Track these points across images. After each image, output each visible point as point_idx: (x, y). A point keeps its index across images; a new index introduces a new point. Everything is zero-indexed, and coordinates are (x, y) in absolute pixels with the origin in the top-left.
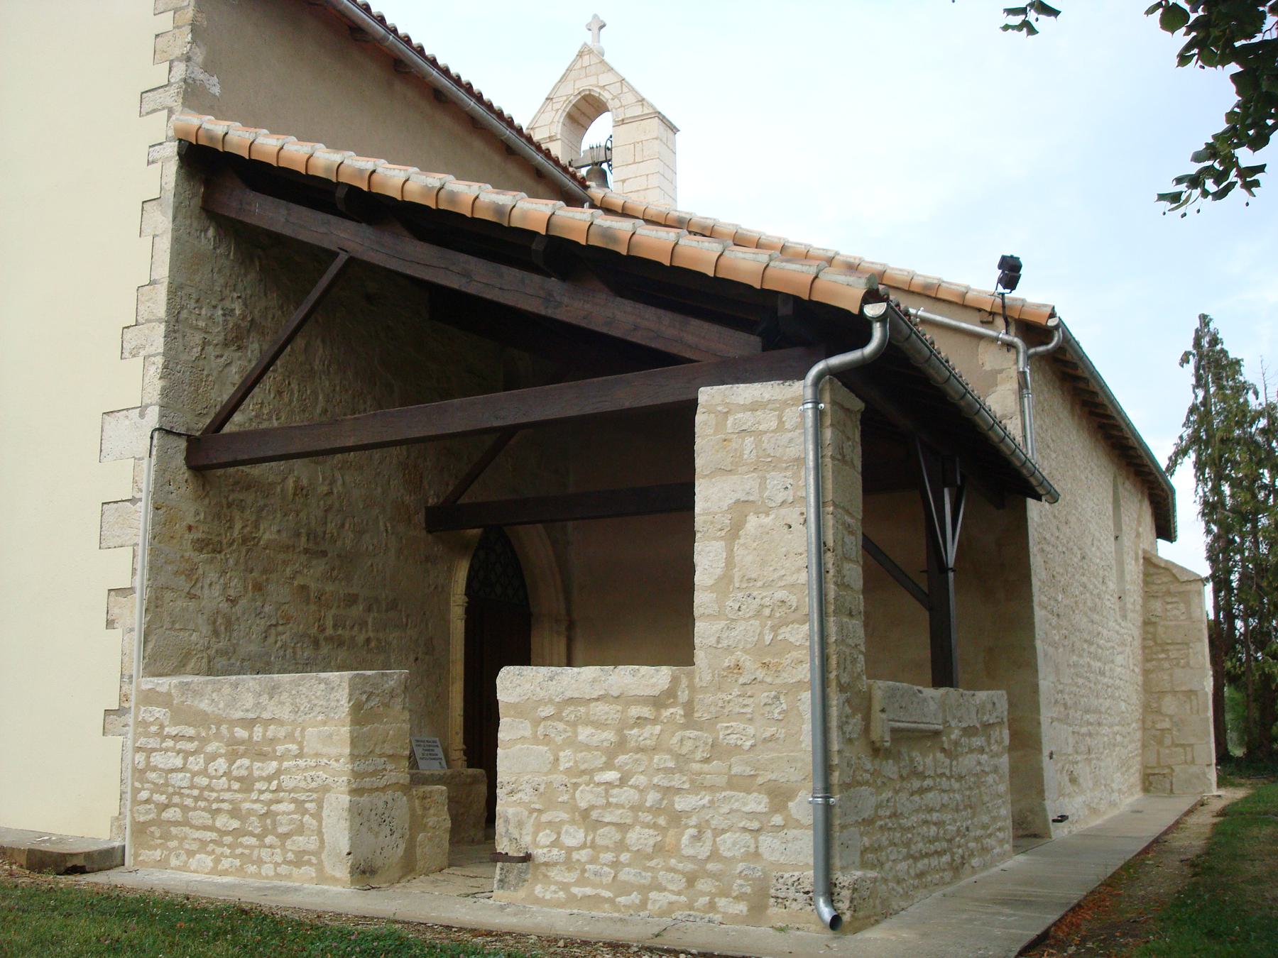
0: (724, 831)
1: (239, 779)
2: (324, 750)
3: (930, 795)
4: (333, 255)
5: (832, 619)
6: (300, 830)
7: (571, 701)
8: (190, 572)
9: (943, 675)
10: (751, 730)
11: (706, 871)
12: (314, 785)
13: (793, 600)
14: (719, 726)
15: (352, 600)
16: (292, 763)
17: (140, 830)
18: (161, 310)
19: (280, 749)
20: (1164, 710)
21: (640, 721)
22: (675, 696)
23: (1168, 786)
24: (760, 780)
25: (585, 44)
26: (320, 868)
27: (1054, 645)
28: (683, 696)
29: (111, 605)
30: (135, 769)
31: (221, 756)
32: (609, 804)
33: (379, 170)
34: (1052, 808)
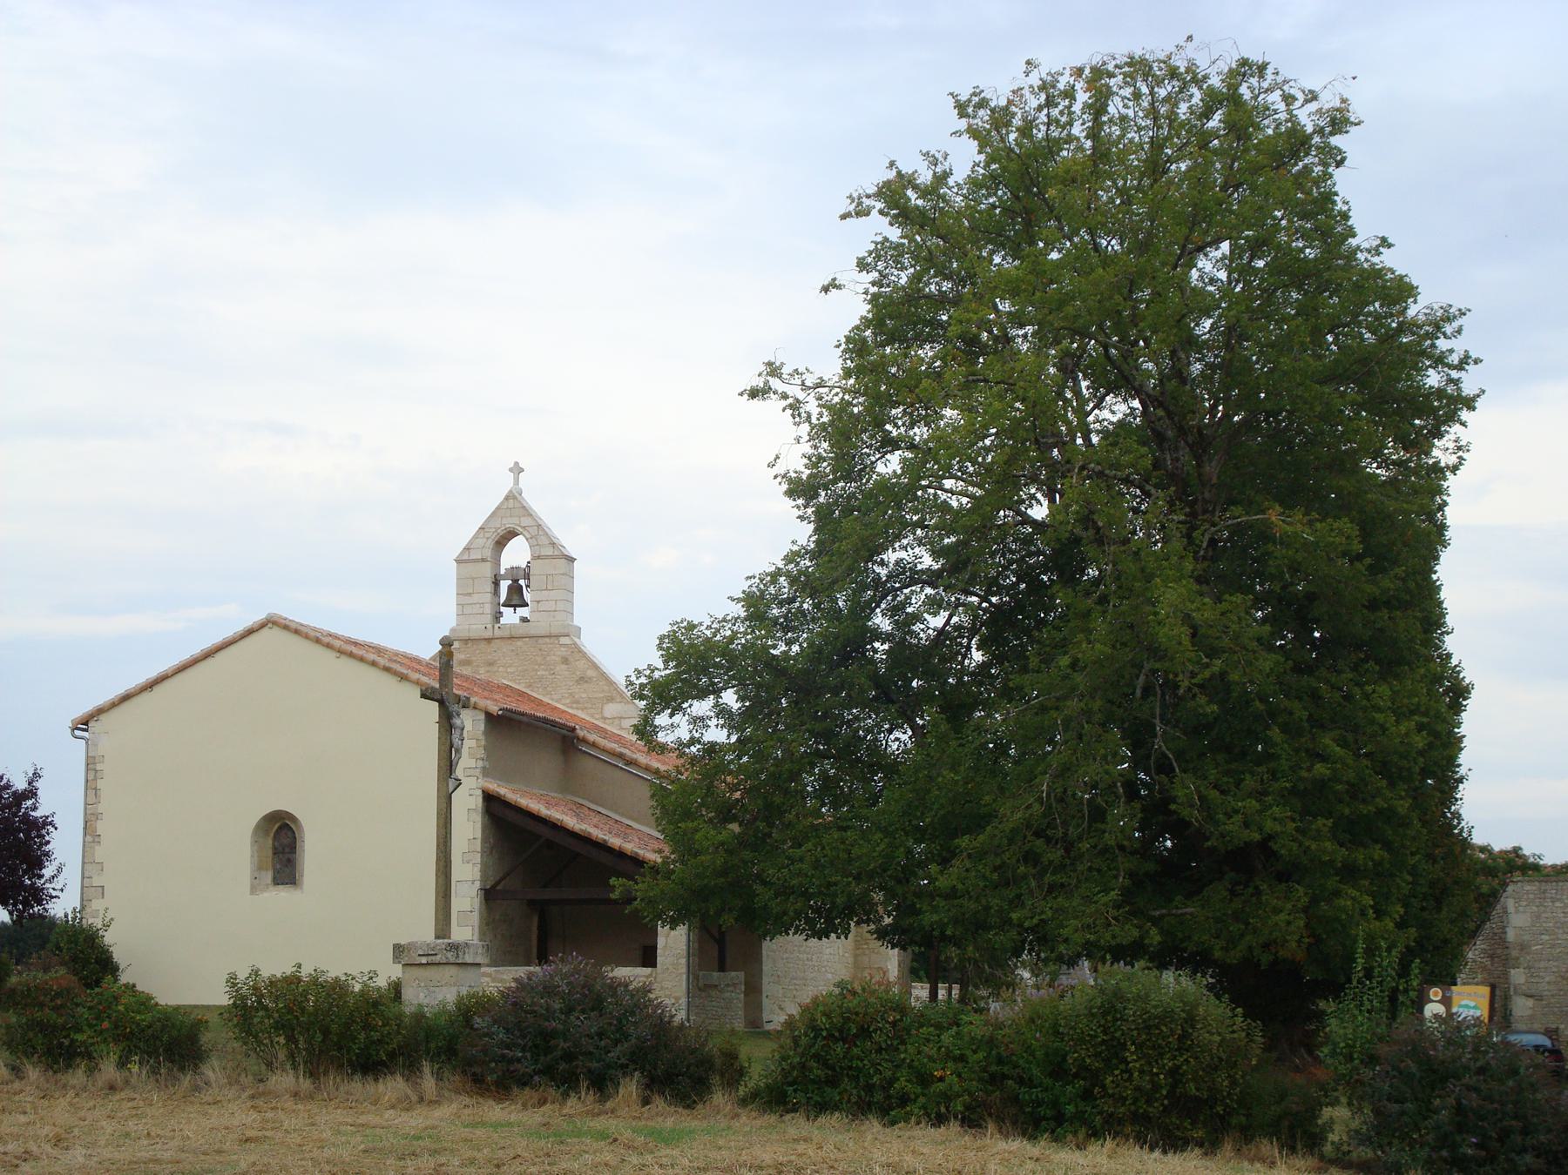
9: (722, 968)
34: (765, 1017)
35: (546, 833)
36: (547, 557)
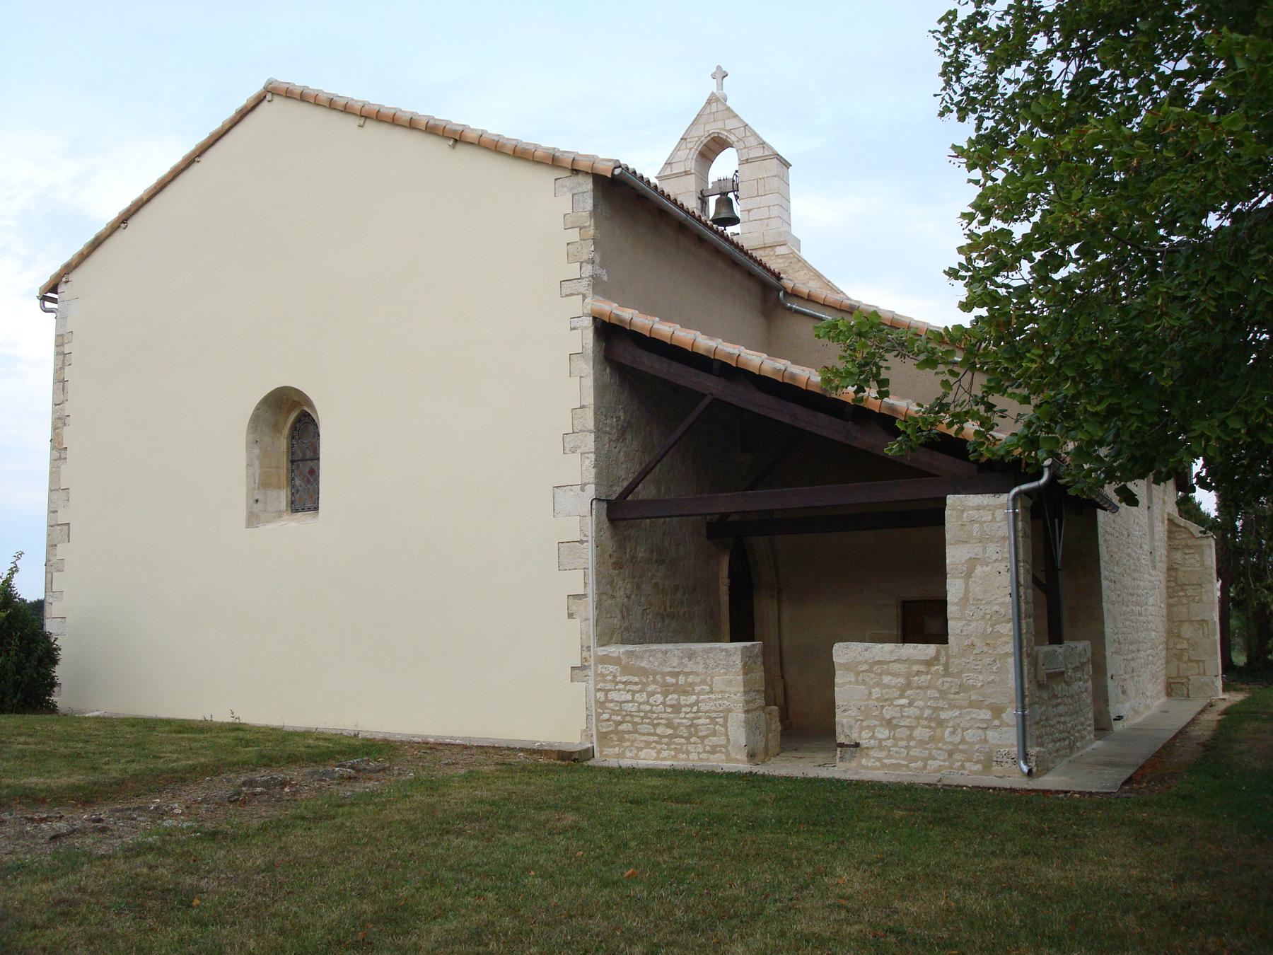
0: (967, 729)
1: (670, 706)
2: (728, 689)
3: (1060, 707)
4: (704, 395)
5: (1024, 621)
6: (714, 734)
7: (878, 662)
8: (611, 583)
10: (981, 677)
11: (958, 749)
12: (721, 708)
13: (1002, 611)
14: (963, 675)
15: (676, 589)
16: (706, 696)
17: (603, 737)
18: (590, 424)
19: (697, 689)
20: (1183, 634)
21: (919, 673)
22: (939, 660)
23: (1185, 692)
24: (987, 703)
25: (713, 93)
26: (727, 753)
27: (1113, 603)
28: (943, 660)
29: (570, 604)
30: (597, 702)
31: (658, 693)
32: (902, 716)
33: (742, 354)
35: (712, 385)
36: (757, 159)
